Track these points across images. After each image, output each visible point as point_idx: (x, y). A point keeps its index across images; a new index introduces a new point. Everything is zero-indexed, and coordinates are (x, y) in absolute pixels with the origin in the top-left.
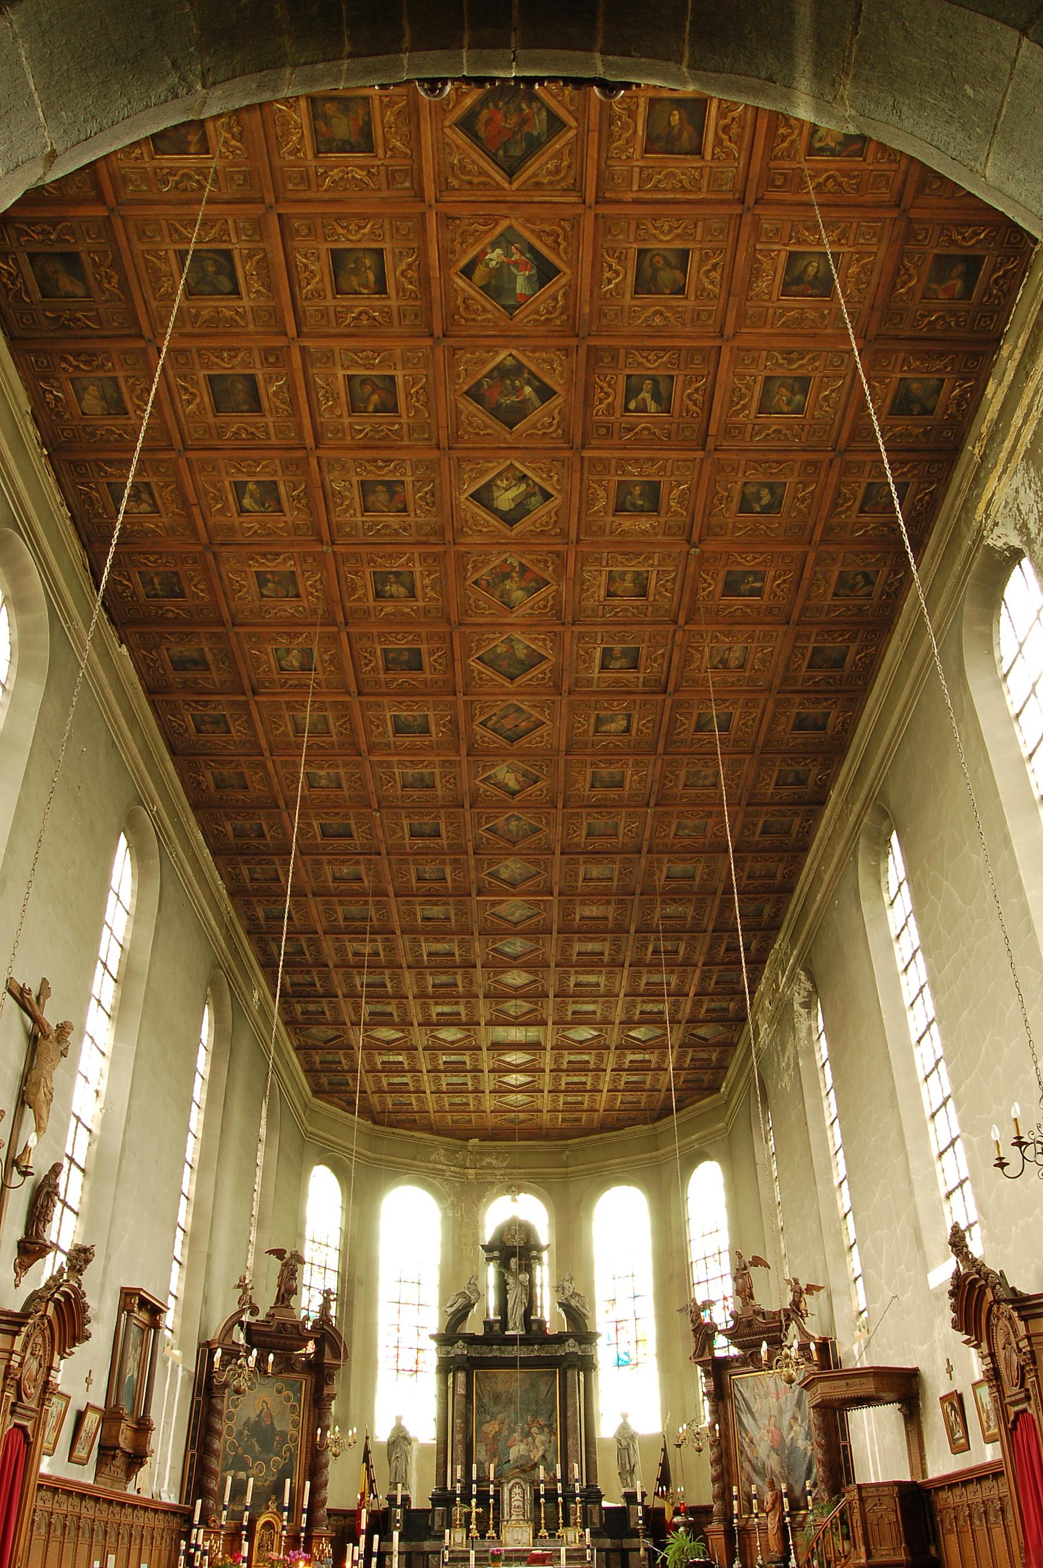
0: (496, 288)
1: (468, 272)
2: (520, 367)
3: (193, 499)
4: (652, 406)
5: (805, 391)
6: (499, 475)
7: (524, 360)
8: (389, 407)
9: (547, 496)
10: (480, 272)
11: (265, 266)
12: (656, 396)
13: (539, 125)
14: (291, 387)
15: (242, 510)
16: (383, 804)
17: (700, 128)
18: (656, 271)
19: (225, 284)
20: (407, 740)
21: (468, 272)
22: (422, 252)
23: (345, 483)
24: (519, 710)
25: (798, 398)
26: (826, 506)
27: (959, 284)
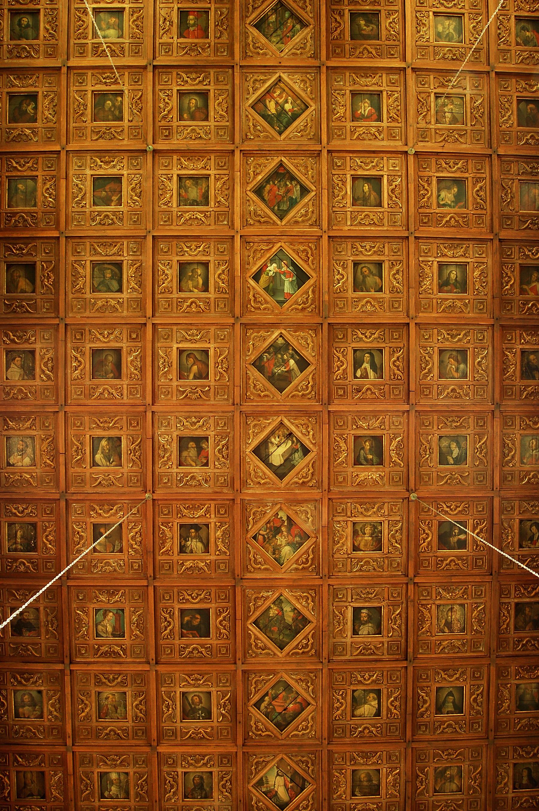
0: (273, 289)
1: (256, 277)
2: (287, 344)
3: (62, 450)
4: (371, 374)
5: (465, 362)
6: (272, 433)
8: (203, 375)
9: (306, 451)
10: (264, 278)
12: (373, 366)
13: (296, 192)
15: (94, 464)
18: (364, 277)
19: (115, 285)
20: (193, 726)
24: (288, 687)
25: (462, 366)
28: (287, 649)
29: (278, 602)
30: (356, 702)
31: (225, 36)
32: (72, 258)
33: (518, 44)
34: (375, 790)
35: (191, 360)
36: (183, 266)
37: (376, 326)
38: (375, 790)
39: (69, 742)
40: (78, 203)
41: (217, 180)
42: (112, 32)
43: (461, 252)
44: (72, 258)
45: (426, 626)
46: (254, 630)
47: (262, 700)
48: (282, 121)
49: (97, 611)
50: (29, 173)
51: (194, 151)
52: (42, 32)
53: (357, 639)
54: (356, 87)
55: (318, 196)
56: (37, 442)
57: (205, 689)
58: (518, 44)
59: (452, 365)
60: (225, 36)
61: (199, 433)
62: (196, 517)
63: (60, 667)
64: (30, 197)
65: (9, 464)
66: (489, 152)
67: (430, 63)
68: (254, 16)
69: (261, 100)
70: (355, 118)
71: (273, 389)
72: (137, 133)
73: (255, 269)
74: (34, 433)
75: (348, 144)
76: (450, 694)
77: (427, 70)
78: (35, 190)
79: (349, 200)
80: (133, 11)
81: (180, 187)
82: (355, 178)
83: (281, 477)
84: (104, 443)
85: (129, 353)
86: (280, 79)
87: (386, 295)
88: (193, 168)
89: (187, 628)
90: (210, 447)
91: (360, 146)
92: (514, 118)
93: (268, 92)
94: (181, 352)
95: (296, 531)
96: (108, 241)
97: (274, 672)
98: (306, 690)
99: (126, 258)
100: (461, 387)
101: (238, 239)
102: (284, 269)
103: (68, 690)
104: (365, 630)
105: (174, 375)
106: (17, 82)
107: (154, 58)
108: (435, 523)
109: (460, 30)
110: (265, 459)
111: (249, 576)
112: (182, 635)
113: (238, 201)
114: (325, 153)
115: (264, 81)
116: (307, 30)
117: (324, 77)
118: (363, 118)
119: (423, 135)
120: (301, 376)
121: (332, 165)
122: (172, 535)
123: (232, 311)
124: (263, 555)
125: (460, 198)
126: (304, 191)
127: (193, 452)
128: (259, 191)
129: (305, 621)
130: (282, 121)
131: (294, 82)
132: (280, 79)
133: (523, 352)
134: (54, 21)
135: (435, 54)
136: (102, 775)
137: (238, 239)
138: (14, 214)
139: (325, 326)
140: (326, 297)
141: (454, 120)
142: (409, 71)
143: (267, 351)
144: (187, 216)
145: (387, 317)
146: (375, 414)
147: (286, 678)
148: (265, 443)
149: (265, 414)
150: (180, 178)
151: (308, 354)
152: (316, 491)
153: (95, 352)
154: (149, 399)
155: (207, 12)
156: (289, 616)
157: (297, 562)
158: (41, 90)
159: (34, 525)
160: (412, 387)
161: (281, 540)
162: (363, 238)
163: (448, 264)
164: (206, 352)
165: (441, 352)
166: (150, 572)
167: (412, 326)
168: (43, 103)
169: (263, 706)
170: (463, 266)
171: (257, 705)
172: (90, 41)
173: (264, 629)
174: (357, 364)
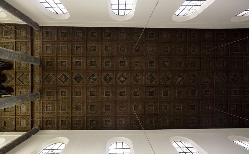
0: (95, 80)
2: (104, 78)
3: (122, 116)
4: (109, 63)
5: (107, 47)
6: (119, 80)
7: (104, 77)
8: (109, 92)
9: (122, 74)
10: (93, 81)
12: (108, 63)
14: (107, 102)
15: (124, 110)
16: (151, 93)
18: (93, 64)
19: (94, 107)
23: (120, 98)
24: (163, 78)
25: (108, 47)
26: (123, 41)
27: (95, 34)
28: (156, 78)
29: (148, 79)
30: (166, 66)
31: (51, 88)
32: (90, 114)
33: (52, 36)
34: (181, 62)
35: (107, 94)
36: (91, 95)
37: (101, 62)
38: (181, 62)
39: (171, 115)
40: (80, 113)
41: (76, 89)
42: (51, 108)
43: (89, 47)
44: (90, 114)
45: (153, 54)
46: (152, 83)
47: (165, 82)
48: (66, 78)
49: (149, 110)
50: (75, 122)
51: (72, 94)
52: (51, 120)
53: (154, 66)
54: (60, 65)
55: (79, 72)
56: (120, 120)
57: (162, 92)
58: (52, 36)
59: (108, 49)
60: (51, 88)
61: (119, 92)
62: (133, 93)
63: (158, 116)
64: (80, 121)
65: (124, 124)
66: (71, 42)
67: (56, 52)
68: (48, 83)
69: (63, 82)
70: (66, 66)
71: (112, 80)
72: (68, 103)
73: (92, 83)
74: (119, 120)
75: (70, 67)
76: (165, 49)
77: (57, 53)
78: (78, 120)
79: (80, 67)
80: (47, 104)
81: (78, 96)
82: (76, 66)
83: (127, 79)
84: (121, 108)
85: (106, 104)
86: (59, 79)
87: (96, 61)
88: (75, 94)
89: (152, 95)
90: (122, 90)
91: (70, 65)
92: (65, 37)
93: (61, 81)
94: (105, 96)
95: (136, 76)
96: (87, 108)
97: (160, 80)
98: (163, 74)
99: (90, 105)
100: (112, 48)
101: (87, 86)
102: (92, 78)
103: (162, 115)
104: (153, 64)
105: (109, 97)
106: (59, 124)
107: (55, 100)
108: (135, 52)
109: (49, 47)
110: (124, 81)
111: (143, 84)
112: (153, 95)
113: (80, 86)
114: (72, 71)
115: (59, 81)
117: (58, 71)
118: (66, 64)
119: (68, 54)
120: (110, 75)
122: (136, 97)
123: (99, 87)
124: (140, 82)
125: (80, 47)
126: (78, 74)
127: (123, 94)
128: (78, 82)
129: (151, 74)
130: (66, 78)
131: (59, 76)
132: (59, 79)
133: (106, 36)
134: (48, 118)
135: (54, 51)
136: (177, 109)
137: (87, 86)
138: (82, 124)
139: (101, 71)
140: (96, 71)
141: (66, 48)
142: (57, 56)
143: (105, 81)
144: (83, 94)
145: (100, 61)
146: (116, 62)
147: (161, 78)
148: (121, 81)
149: (116, 81)
150: (76, 96)
151: (106, 74)
152: (129, 73)
153: (106, 110)
154: (114, 101)
155: (47, 91)
156: (150, 77)
157: (141, 76)
158: (61, 120)
159: (134, 120)
160: (112, 56)
161: (137, 79)
162: (86, 64)
163: (91, 50)
164: (106, 91)
165: (106, 51)
166: (142, 101)
167: (102, 56)
168: (63, 119)
169: (166, 82)
170: (91, 47)
171: (165, 83)
172: (52, 111)
173: (153, 82)
174: (108, 65)
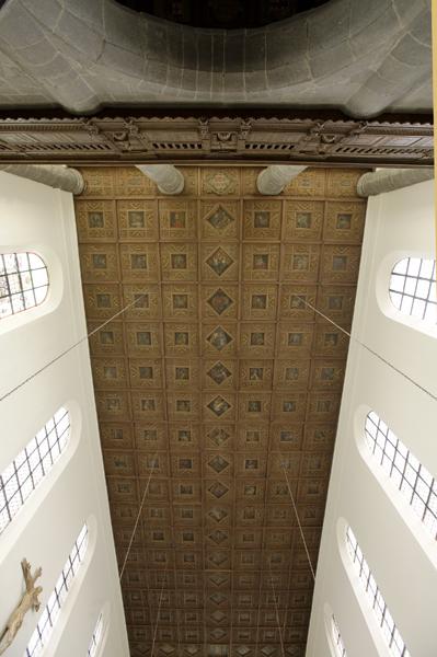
1: (209, 339)
9: (229, 406)
11: (158, 336)
13: (227, 302)
15: (144, 409)
17: (265, 302)
20: (185, 496)
21: (209, 339)
22: (198, 332)
23: (173, 401)
29: (217, 457)
46: (207, 466)
48: (221, 269)
55: (237, 305)
60: (193, 227)
62: (185, 429)
69: (211, 258)
83: (219, 415)
89: (182, 466)
93: (214, 255)
116: (234, 223)
121: (243, 290)
122: (176, 435)
126: (231, 301)
128: (210, 302)
130: (221, 269)
131: (227, 250)
148: (213, 403)
161: (218, 437)
174: (251, 374)
